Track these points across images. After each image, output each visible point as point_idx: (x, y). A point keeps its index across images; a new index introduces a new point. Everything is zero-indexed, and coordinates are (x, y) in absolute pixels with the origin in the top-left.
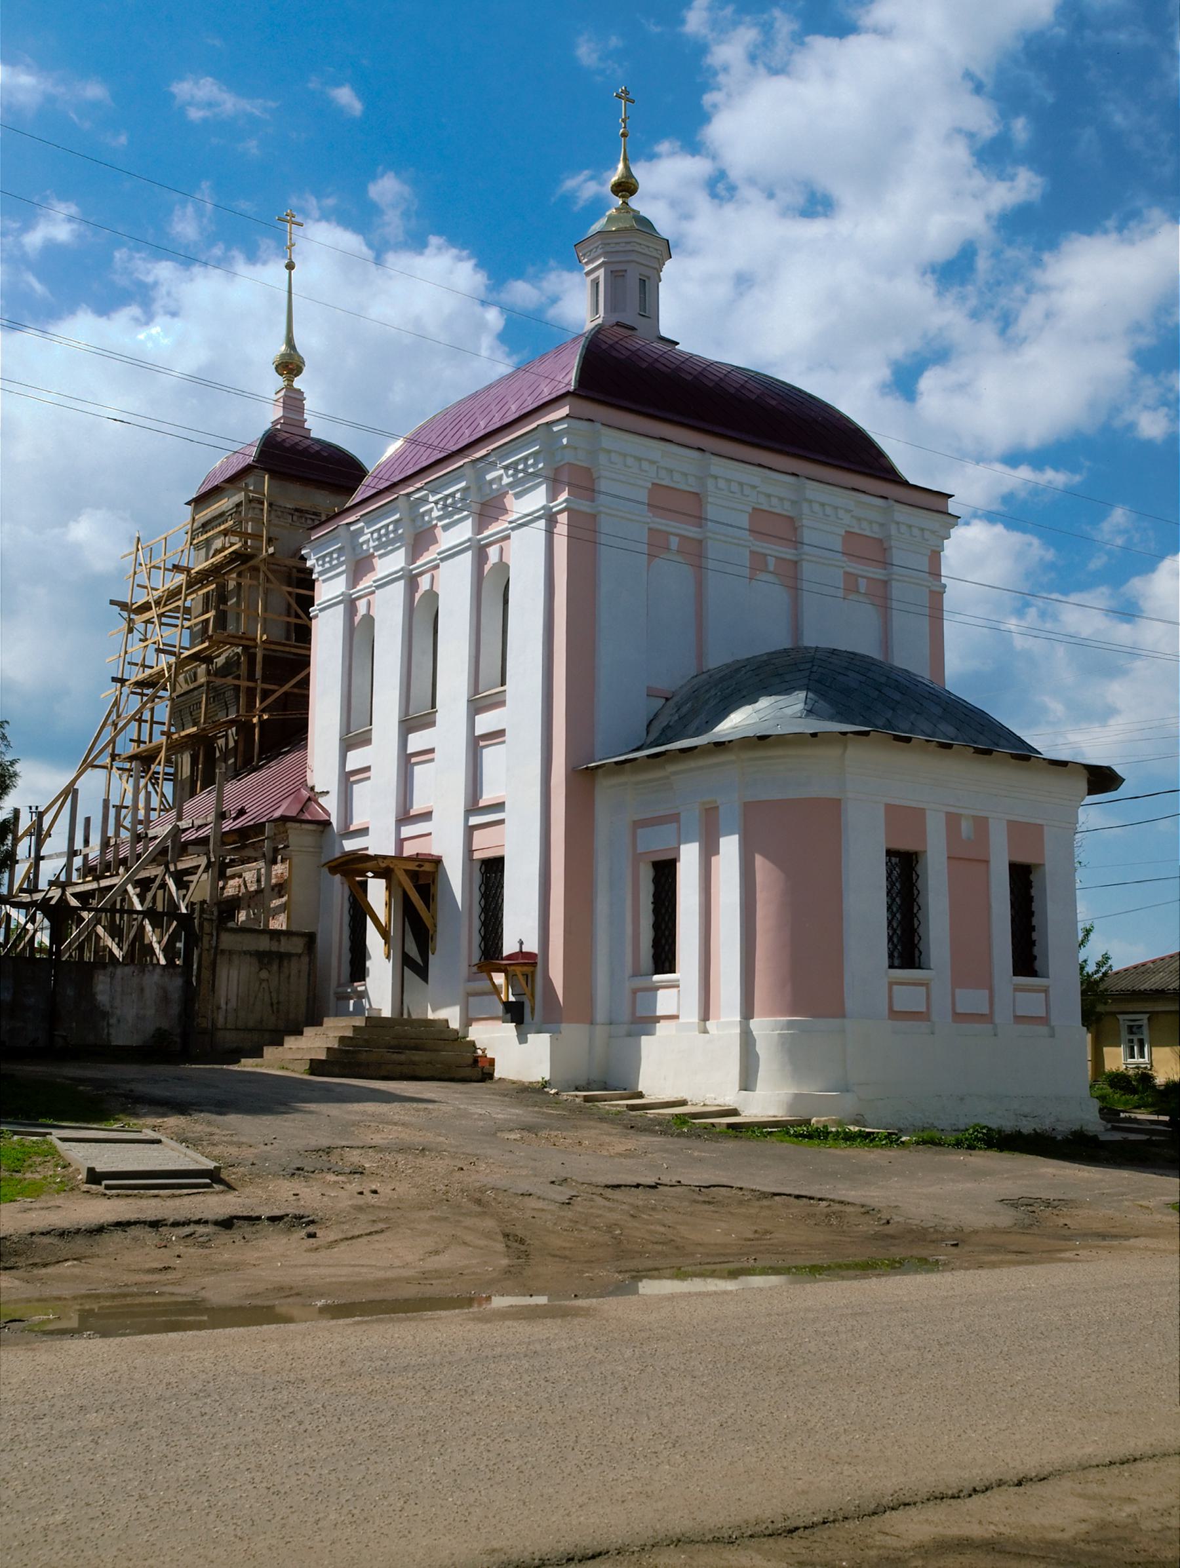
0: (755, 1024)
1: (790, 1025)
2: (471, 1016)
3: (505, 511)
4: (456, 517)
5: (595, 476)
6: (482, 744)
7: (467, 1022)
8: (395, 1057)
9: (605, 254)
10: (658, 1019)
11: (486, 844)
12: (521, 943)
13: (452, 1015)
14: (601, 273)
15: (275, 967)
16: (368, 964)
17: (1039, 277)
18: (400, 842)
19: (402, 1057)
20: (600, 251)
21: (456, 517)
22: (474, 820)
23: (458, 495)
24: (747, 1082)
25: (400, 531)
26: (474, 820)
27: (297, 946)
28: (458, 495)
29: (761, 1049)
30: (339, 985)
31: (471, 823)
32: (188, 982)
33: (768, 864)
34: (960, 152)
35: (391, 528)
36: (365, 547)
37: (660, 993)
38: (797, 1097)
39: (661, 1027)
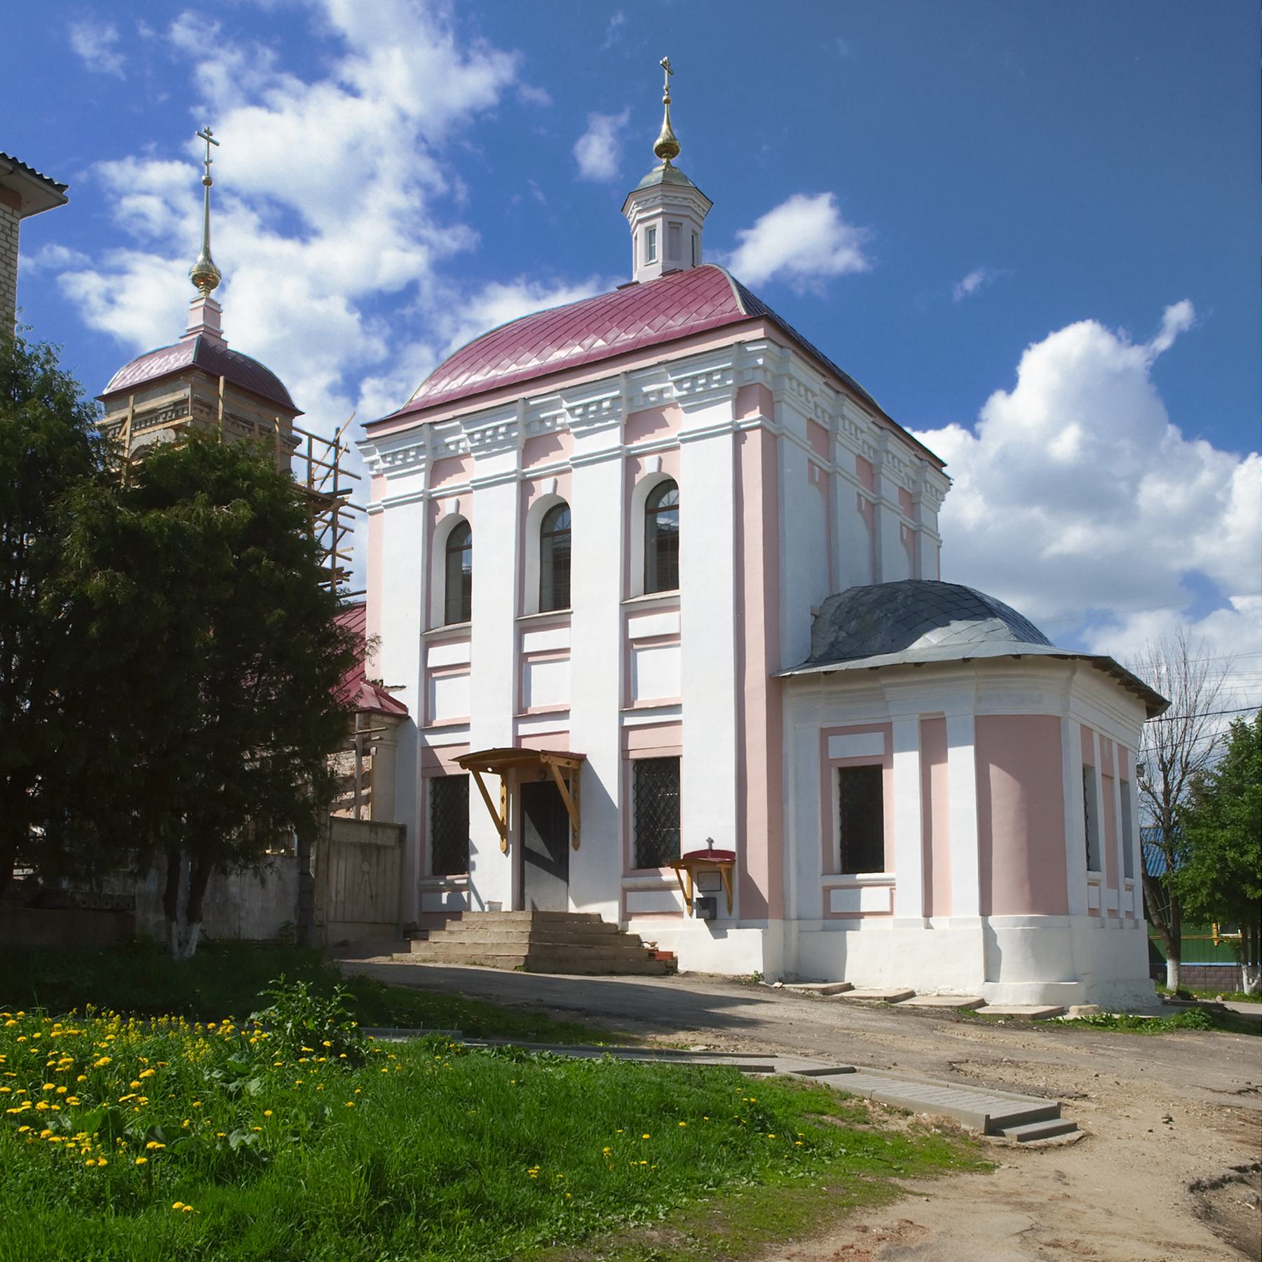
0: (993, 920)
1: (1032, 921)
2: (629, 910)
3: (663, 424)
4: (597, 425)
5: (775, 399)
6: (635, 647)
7: (626, 916)
8: (586, 951)
9: (664, 205)
11: (647, 745)
12: (711, 841)
13: (609, 912)
14: (659, 222)
15: (374, 860)
16: (473, 858)
17: (465, 313)
18: (518, 739)
19: (593, 952)
20: (658, 201)
21: (597, 425)
23: (606, 404)
24: (991, 972)
25: (514, 434)
26: (629, 721)
27: (388, 838)
28: (606, 404)
29: (1002, 943)
30: (422, 877)
31: (626, 724)
32: (304, 874)
33: (1004, 775)
34: (415, 201)
35: (502, 430)
36: (452, 447)
37: (864, 890)
38: (1048, 987)
39: (864, 922)
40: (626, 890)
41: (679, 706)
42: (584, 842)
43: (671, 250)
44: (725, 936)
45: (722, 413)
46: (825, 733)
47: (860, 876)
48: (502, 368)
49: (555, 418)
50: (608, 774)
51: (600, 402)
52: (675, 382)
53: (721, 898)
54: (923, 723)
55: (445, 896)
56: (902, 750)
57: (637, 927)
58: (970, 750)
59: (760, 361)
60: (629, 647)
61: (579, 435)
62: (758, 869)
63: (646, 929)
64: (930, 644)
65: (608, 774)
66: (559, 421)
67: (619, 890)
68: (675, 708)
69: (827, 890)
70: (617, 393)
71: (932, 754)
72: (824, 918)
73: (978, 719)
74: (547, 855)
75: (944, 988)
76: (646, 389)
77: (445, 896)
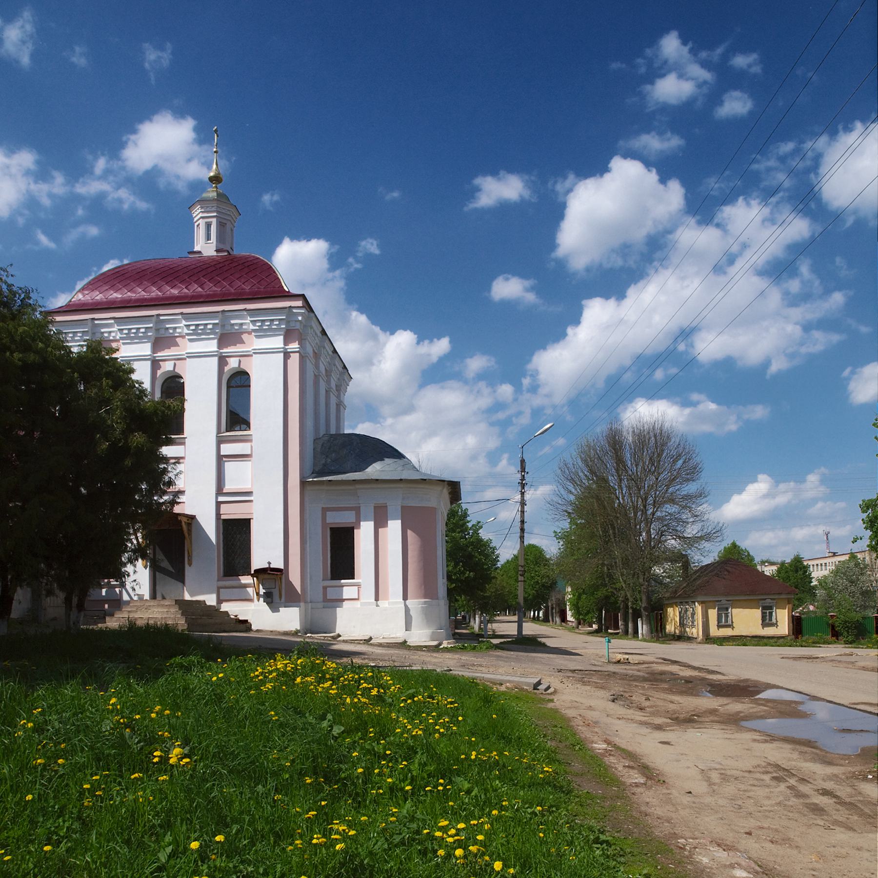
10: (344, 600)
11: (231, 512)
12: (269, 563)
13: (211, 600)
14: (214, 220)
22: (221, 499)
24: (408, 627)
26: (221, 499)
28: (210, 327)
37: (345, 588)
40: (219, 588)
41: (252, 492)
42: (194, 563)
43: (220, 238)
44: (279, 611)
45: (277, 342)
46: (325, 510)
47: (343, 581)
48: (135, 292)
49: (175, 328)
50: (210, 527)
51: (207, 324)
52: (251, 321)
53: (276, 593)
54: (375, 507)
55: (104, 591)
56: (365, 521)
57: (225, 607)
58: (372, 523)
59: (300, 318)
60: (221, 459)
61: (191, 340)
62: (295, 577)
63: (232, 608)
64: (375, 470)
65: (210, 527)
66: (178, 330)
67: (216, 589)
68: (249, 493)
69: (325, 588)
70: (217, 321)
71: (380, 523)
72: (324, 601)
73: (403, 508)
74: (171, 569)
75: (386, 634)
76: (233, 322)
77: (104, 591)
